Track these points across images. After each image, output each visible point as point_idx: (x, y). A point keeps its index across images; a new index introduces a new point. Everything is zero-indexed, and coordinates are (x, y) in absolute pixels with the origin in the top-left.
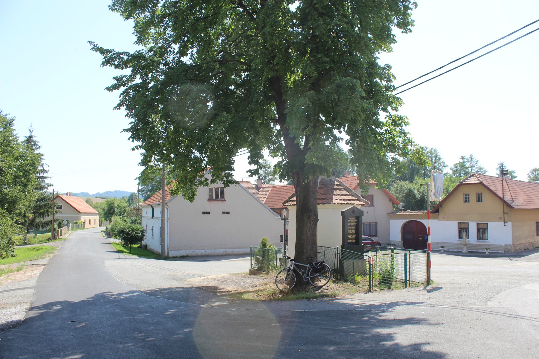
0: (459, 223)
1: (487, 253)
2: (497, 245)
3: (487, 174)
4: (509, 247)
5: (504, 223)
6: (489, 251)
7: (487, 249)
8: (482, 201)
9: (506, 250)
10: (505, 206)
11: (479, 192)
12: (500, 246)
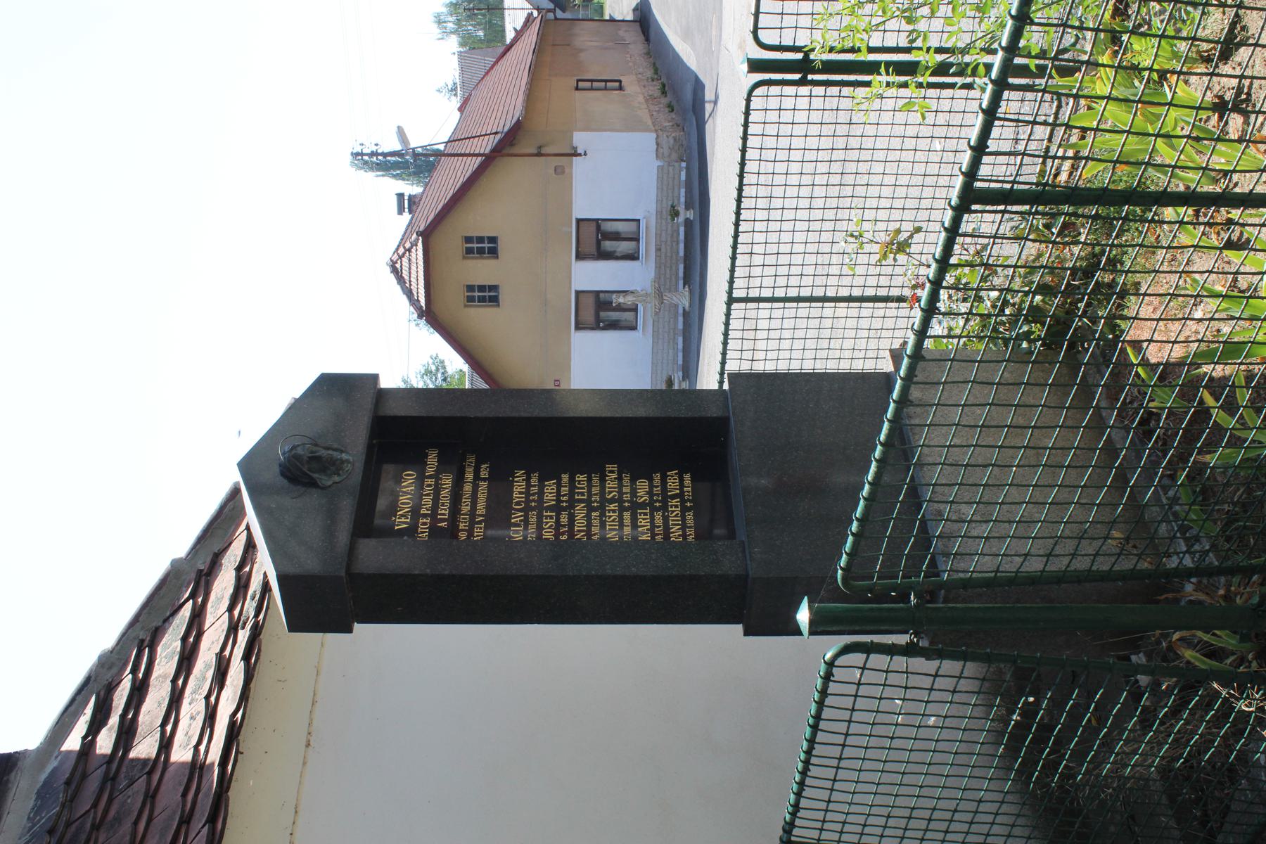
0: (579, 327)
1: (690, 215)
2: (660, 188)
3: (739, 628)
4: (667, 142)
5: (576, 154)
6: (681, 208)
7: (675, 214)
8: (493, 240)
9: (674, 156)
10: (516, 150)
11: (460, 246)
12: (660, 179)
